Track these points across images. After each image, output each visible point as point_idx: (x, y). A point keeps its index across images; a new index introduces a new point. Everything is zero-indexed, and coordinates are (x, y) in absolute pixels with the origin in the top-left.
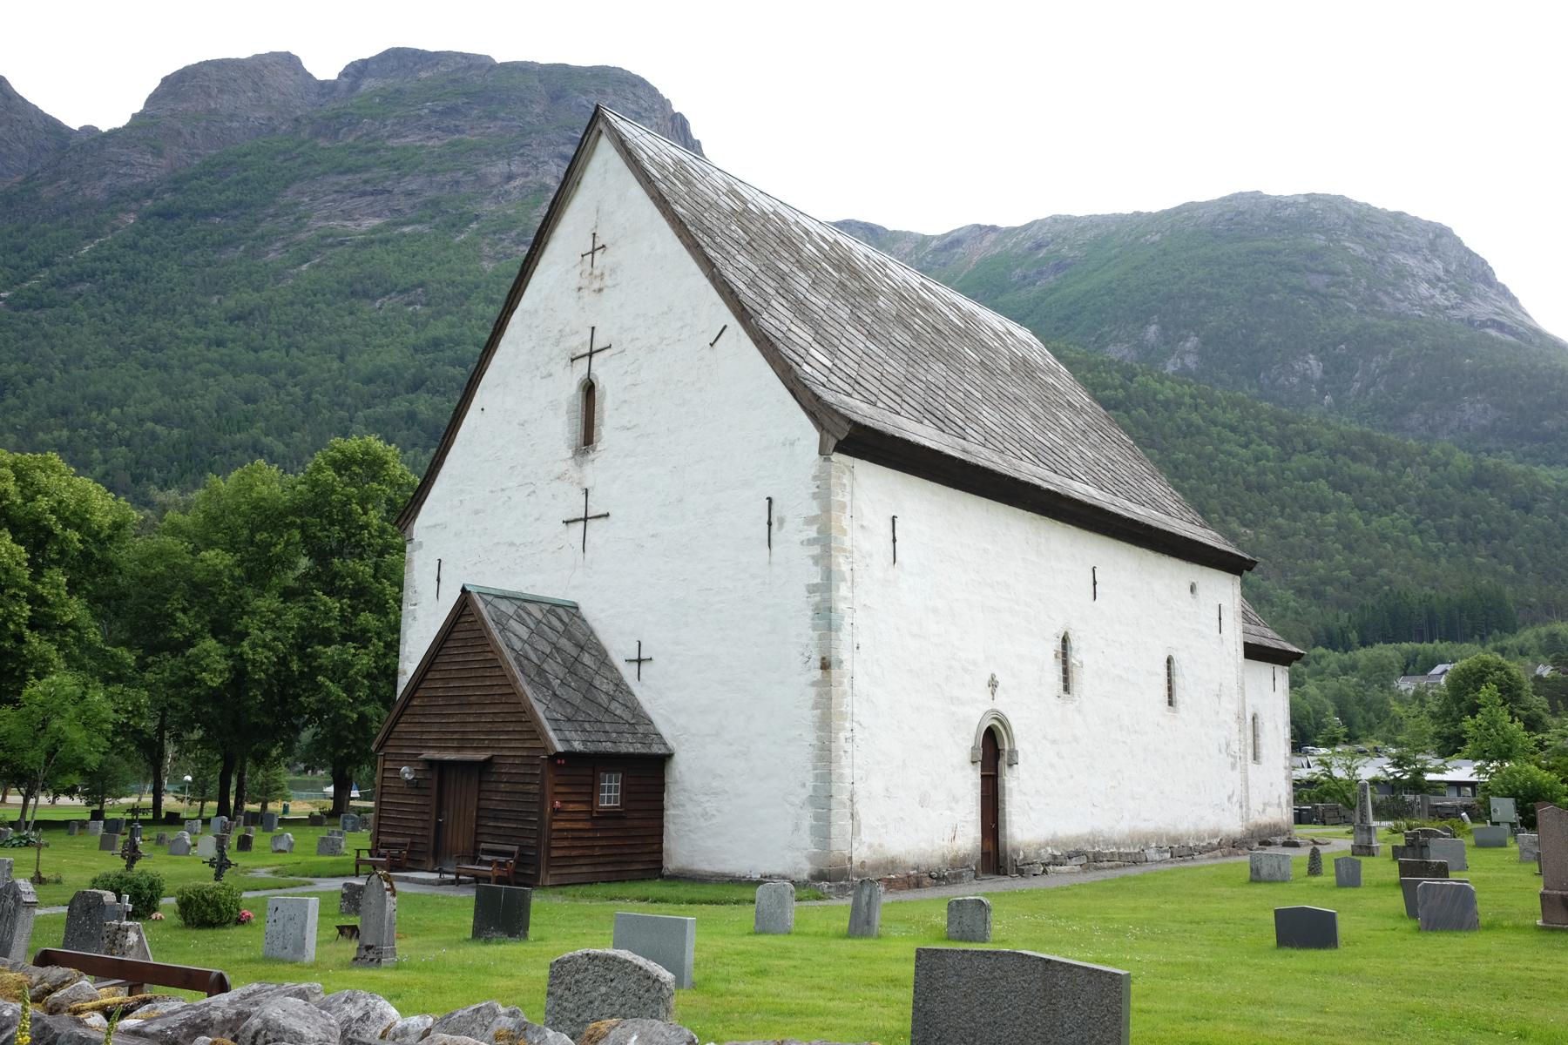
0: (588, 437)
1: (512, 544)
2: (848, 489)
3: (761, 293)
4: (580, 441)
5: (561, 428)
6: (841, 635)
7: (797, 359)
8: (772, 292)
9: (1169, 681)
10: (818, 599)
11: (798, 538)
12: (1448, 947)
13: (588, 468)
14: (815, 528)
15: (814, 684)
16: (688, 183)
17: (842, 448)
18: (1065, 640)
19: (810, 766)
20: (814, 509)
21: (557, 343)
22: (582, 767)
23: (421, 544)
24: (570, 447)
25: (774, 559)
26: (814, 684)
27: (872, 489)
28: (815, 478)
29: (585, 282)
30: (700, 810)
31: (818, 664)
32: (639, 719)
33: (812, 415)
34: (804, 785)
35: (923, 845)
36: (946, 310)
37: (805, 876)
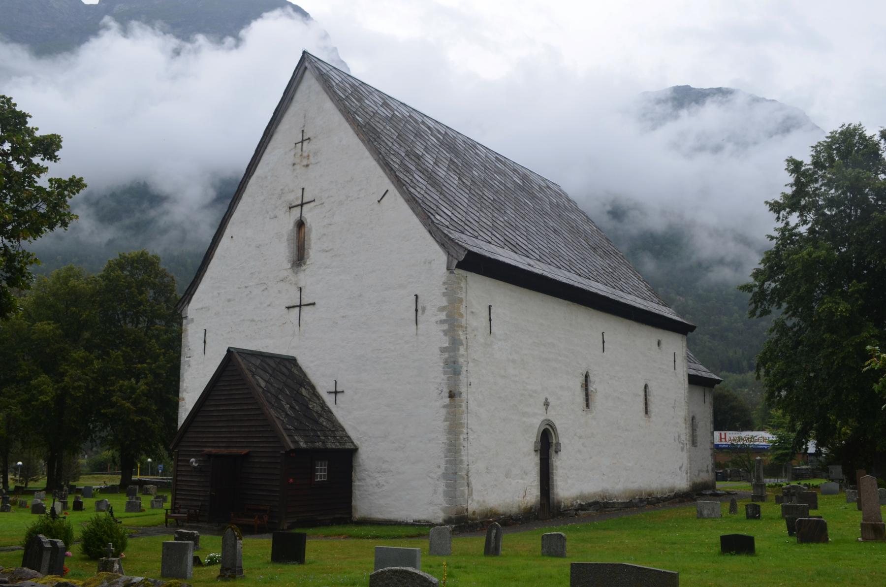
0: (300, 257)
1: (253, 321)
2: (464, 290)
3: (408, 170)
4: (295, 258)
5: (283, 251)
6: (461, 377)
7: (432, 211)
8: (414, 169)
9: (646, 399)
10: (447, 356)
11: (434, 319)
12: (812, 552)
13: (301, 275)
14: (445, 313)
15: (445, 407)
16: (360, 100)
17: (461, 265)
18: (587, 376)
19: (443, 456)
20: (444, 302)
21: (280, 197)
22: (304, 459)
23: (192, 320)
24: (289, 262)
25: (419, 332)
26: (445, 407)
27: (479, 290)
28: (444, 283)
29: (297, 160)
30: (374, 482)
31: (447, 395)
32: (336, 428)
33: (442, 245)
34: (439, 467)
35: (508, 500)
36: (511, 173)
37: (440, 521)
